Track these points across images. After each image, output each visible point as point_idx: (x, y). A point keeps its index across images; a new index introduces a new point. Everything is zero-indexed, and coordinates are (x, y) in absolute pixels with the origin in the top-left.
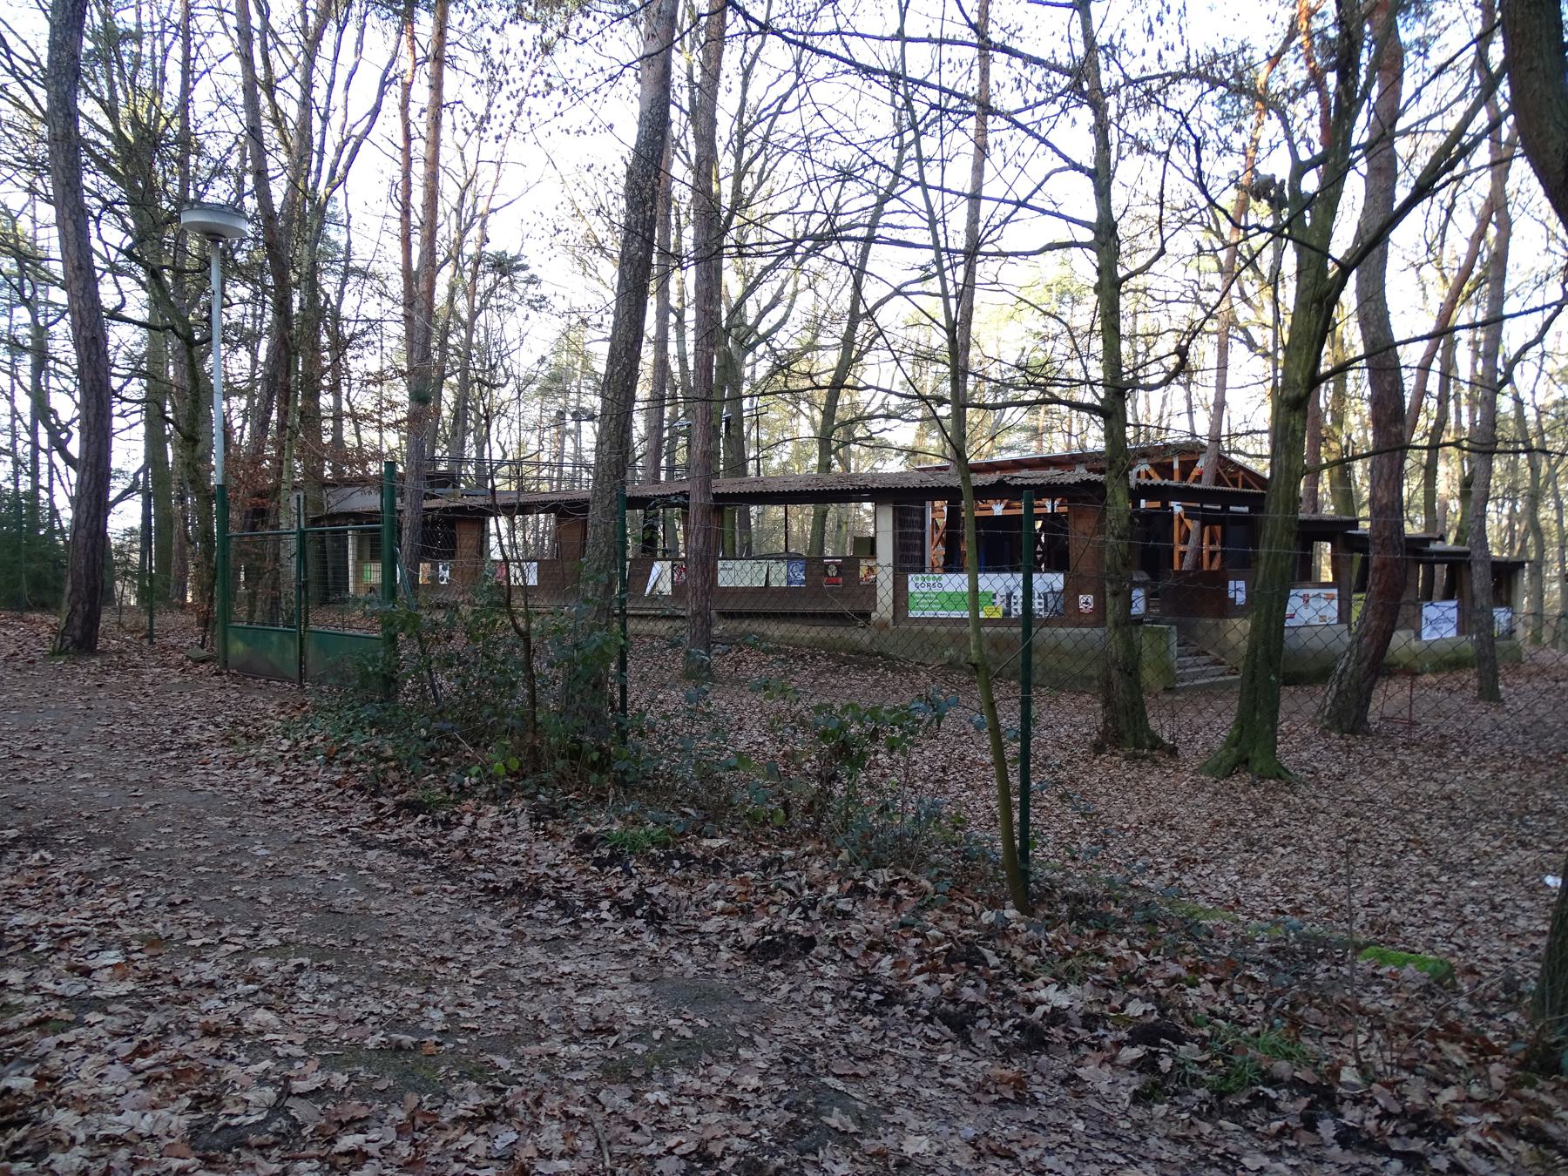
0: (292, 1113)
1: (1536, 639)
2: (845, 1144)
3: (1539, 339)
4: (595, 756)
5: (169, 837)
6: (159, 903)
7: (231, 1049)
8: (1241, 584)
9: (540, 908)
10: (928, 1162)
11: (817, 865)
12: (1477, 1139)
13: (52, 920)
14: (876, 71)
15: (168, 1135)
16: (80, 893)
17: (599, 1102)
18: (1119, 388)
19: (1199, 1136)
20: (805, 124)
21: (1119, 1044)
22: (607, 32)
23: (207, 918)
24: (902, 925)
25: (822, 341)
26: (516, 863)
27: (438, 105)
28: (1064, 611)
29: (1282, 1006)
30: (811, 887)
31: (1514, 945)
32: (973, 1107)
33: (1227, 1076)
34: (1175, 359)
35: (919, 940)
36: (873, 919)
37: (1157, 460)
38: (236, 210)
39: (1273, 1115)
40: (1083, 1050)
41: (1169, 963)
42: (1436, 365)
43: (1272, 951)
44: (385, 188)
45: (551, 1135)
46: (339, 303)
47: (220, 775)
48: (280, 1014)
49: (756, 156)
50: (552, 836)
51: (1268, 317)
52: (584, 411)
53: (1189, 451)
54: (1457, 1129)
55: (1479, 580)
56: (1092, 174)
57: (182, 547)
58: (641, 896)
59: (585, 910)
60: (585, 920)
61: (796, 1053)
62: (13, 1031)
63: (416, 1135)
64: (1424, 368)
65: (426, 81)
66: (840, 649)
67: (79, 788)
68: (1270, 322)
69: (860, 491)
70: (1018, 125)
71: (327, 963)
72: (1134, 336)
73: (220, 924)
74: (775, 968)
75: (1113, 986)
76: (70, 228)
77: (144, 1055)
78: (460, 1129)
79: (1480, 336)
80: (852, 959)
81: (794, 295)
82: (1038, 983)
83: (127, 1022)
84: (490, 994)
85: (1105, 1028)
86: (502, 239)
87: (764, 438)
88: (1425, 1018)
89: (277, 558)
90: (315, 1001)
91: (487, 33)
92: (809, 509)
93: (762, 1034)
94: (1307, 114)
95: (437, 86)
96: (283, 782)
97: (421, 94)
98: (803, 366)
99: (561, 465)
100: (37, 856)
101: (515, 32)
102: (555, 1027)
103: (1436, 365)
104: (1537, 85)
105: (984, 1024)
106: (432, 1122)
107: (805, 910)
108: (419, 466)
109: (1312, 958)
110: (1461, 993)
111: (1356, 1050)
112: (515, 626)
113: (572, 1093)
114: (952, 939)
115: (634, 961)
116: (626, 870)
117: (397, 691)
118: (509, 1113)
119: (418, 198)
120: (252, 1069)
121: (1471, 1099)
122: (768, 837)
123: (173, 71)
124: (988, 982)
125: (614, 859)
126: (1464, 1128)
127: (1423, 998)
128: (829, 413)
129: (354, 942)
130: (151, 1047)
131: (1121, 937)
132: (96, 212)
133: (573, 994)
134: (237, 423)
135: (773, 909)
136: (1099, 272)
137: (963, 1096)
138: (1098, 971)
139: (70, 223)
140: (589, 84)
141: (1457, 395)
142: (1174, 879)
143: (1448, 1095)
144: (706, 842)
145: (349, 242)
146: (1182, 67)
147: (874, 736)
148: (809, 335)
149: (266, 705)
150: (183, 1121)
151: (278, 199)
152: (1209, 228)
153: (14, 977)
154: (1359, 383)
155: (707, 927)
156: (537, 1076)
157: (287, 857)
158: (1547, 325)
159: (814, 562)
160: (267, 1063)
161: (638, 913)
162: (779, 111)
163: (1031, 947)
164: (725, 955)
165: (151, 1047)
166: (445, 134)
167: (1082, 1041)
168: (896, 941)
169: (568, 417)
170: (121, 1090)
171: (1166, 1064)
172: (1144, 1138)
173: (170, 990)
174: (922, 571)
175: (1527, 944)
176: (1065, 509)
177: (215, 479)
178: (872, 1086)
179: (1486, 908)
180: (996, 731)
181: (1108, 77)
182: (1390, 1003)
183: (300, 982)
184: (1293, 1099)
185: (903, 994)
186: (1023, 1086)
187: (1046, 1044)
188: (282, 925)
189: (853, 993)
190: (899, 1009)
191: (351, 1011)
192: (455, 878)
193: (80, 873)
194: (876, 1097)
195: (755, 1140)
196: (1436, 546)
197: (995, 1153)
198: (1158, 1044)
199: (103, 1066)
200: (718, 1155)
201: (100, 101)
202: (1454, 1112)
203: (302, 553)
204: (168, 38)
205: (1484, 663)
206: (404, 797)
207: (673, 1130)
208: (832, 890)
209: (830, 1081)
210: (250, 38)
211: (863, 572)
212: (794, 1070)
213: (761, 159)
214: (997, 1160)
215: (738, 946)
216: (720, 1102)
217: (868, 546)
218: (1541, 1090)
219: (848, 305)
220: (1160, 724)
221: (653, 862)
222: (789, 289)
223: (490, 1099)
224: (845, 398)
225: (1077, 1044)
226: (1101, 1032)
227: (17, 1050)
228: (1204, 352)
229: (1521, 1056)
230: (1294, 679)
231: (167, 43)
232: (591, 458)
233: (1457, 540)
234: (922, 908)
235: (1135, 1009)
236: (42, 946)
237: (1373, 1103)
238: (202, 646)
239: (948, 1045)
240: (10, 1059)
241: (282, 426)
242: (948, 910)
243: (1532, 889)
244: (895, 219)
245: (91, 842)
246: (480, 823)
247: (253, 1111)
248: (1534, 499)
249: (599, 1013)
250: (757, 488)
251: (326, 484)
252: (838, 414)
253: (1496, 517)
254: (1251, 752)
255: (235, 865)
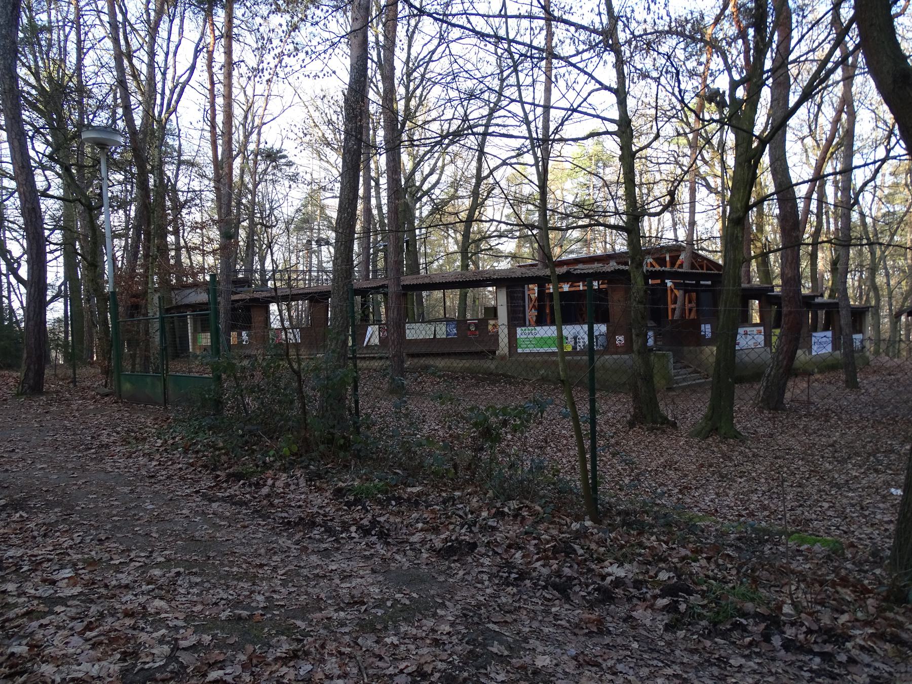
0: (180, 659)
1: (877, 353)
2: (502, 662)
3: (873, 178)
4: (342, 441)
5: (95, 501)
6: (92, 540)
7: (141, 624)
8: (708, 326)
9: (316, 532)
10: (550, 670)
11: (475, 500)
12: (862, 643)
13: (30, 553)
14: (488, 36)
15: (109, 676)
16: (45, 536)
17: (358, 645)
18: (636, 213)
19: (704, 648)
20: (444, 64)
21: (655, 597)
22: (330, 18)
23: (121, 547)
24: (526, 533)
25: (460, 193)
26: (300, 507)
27: (230, 65)
28: (610, 346)
29: (747, 570)
30: (472, 513)
31: (877, 528)
32: (574, 637)
33: (718, 613)
34: (668, 198)
35: (536, 542)
36: (509, 530)
37: (656, 256)
38: (111, 129)
39: (745, 634)
40: (635, 601)
41: (681, 549)
42: (815, 196)
43: (739, 539)
44: (200, 115)
45: (332, 665)
46: (176, 181)
47: (122, 462)
48: (169, 602)
49: (418, 87)
50: (320, 490)
51: (718, 170)
52: (323, 239)
53: (675, 250)
54: (850, 638)
55: (844, 319)
56: (615, 92)
57: (90, 329)
58: (374, 522)
59: (342, 532)
60: (342, 538)
61: (470, 611)
62: (13, 619)
63: (253, 669)
64: (808, 198)
65: (222, 50)
66: (479, 372)
67: (39, 474)
68: (719, 173)
69: (487, 280)
70: (571, 64)
71: (194, 570)
72: (642, 184)
73: (130, 550)
74: (455, 561)
75: (649, 563)
76: (16, 144)
77: (91, 630)
78: (279, 664)
79: (839, 177)
80: (499, 554)
81: (444, 166)
82: (607, 563)
83: (79, 611)
84: (290, 584)
85: (647, 588)
86: (271, 138)
87: (429, 251)
88: (828, 574)
89: (147, 332)
90: (188, 593)
91: (258, 20)
92: (458, 291)
93: (449, 600)
94: (736, 53)
95: (229, 52)
96: (159, 464)
97: (220, 57)
98: (450, 209)
99: (310, 271)
100: (18, 515)
101: (276, 20)
102: (329, 602)
103: (815, 196)
104: (875, 34)
105: (577, 588)
106: (262, 661)
107: (470, 527)
108: (228, 276)
109: (762, 542)
110: (847, 559)
111: (791, 594)
112: (292, 367)
113: (342, 640)
114: (556, 540)
115: (372, 561)
116: (364, 508)
117: (223, 409)
118: (307, 653)
119: (220, 118)
120: (155, 635)
121: (857, 620)
122: (445, 485)
123: (72, 47)
124: (578, 564)
125: (357, 502)
126: (854, 637)
127: (826, 563)
128: (466, 235)
129: (209, 558)
130: (95, 625)
131: (652, 534)
132: (30, 134)
133: (338, 582)
134: (119, 254)
135: (451, 527)
136: (621, 149)
137: (567, 631)
138: (640, 555)
139: (16, 141)
140: (321, 48)
141: (827, 212)
142: (679, 499)
143: (844, 618)
144: (409, 490)
145: (180, 145)
146: (667, 28)
147: (505, 423)
148: (453, 190)
149: (146, 420)
150: (117, 667)
151: (138, 122)
152: (682, 120)
153: (11, 587)
154: (772, 209)
155: (414, 539)
156: (321, 631)
157: (165, 509)
158: (877, 171)
159: (461, 323)
160: (163, 631)
161: (373, 532)
162: (430, 60)
163: (601, 543)
164: (425, 555)
165: (95, 625)
166: (235, 81)
167: (634, 596)
168: (523, 542)
169: (313, 243)
170: (79, 651)
171: (683, 607)
172: (672, 651)
173: (103, 591)
174: (524, 325)
175: (883, 528)
176: (604, 286)
177: (108, 288)
178: (515, 627)
179: (858, 508)
180: (576, 419)
181: (622, 36)
182: (807, 566)
183: (179, 582)
184: (756, 624)
185: (530, 574)
186: (602, 624)
187: (613, 598)
188: (166, 549)
189: (501, 574)
190: (528, 582)
191: (210, 598)
192: (265, 517)
193: (44, 524)
194: (518, 634)
195: (450, 662)
196: (818, 300)
197: (588, 664)
198: (678, 596)
199: (67, 637)
200: (429, 672)
201: (29, 68)
202: (848, 628)
203: (162, 329)
204: (67, 29)
205: (848, 366)
206: (231, 470)
207: (403, 659)
208: (485, 514)
209: (491, 626)
210: (117, 28)
211: (490, 327)
212: (470, 620)
213: (421, 88)
214: (590, 668)
215: (432, 549)
216: (428, 641)
217: (492, 312)
218: (897, 613)
219: (475, 172)
220: (666, 410)
221: (379, 502)
222: (440, 164)
223: (294, 646)
224: (475, 227)
225: (631, 598)
226: (644, 590)
227: (16, 630)
228: (683, 194)
229: (884, 594)
230: (740, 380)
231: (67, 32)
232: (329, 266)
233: (830, 296)
234: (537, 522)
235: (663, 576)
236: (25, 568)
237: (802, 624)
238: (106, 386)
239: (557, 602)
240: (13, 636)
241: (146, 256)
242: (551, 523)
243: (884, 497)
244: (499, 121)
245: (49, 505)
246: (277, 484)
247: (158, 660)
248: (873, 270)
249: (355, 592)
250: (427, 281)
251: (173, 288)
252: (472, 235)
253: (852, 281)
254: (718, 424)
255: (135, 515)
